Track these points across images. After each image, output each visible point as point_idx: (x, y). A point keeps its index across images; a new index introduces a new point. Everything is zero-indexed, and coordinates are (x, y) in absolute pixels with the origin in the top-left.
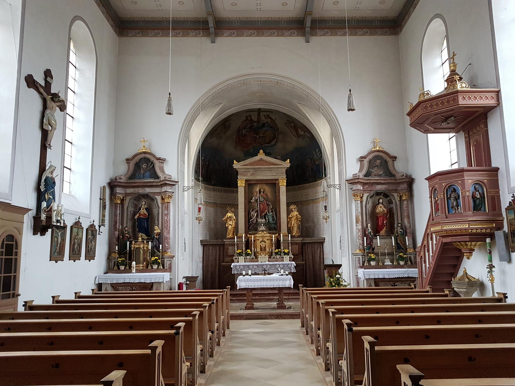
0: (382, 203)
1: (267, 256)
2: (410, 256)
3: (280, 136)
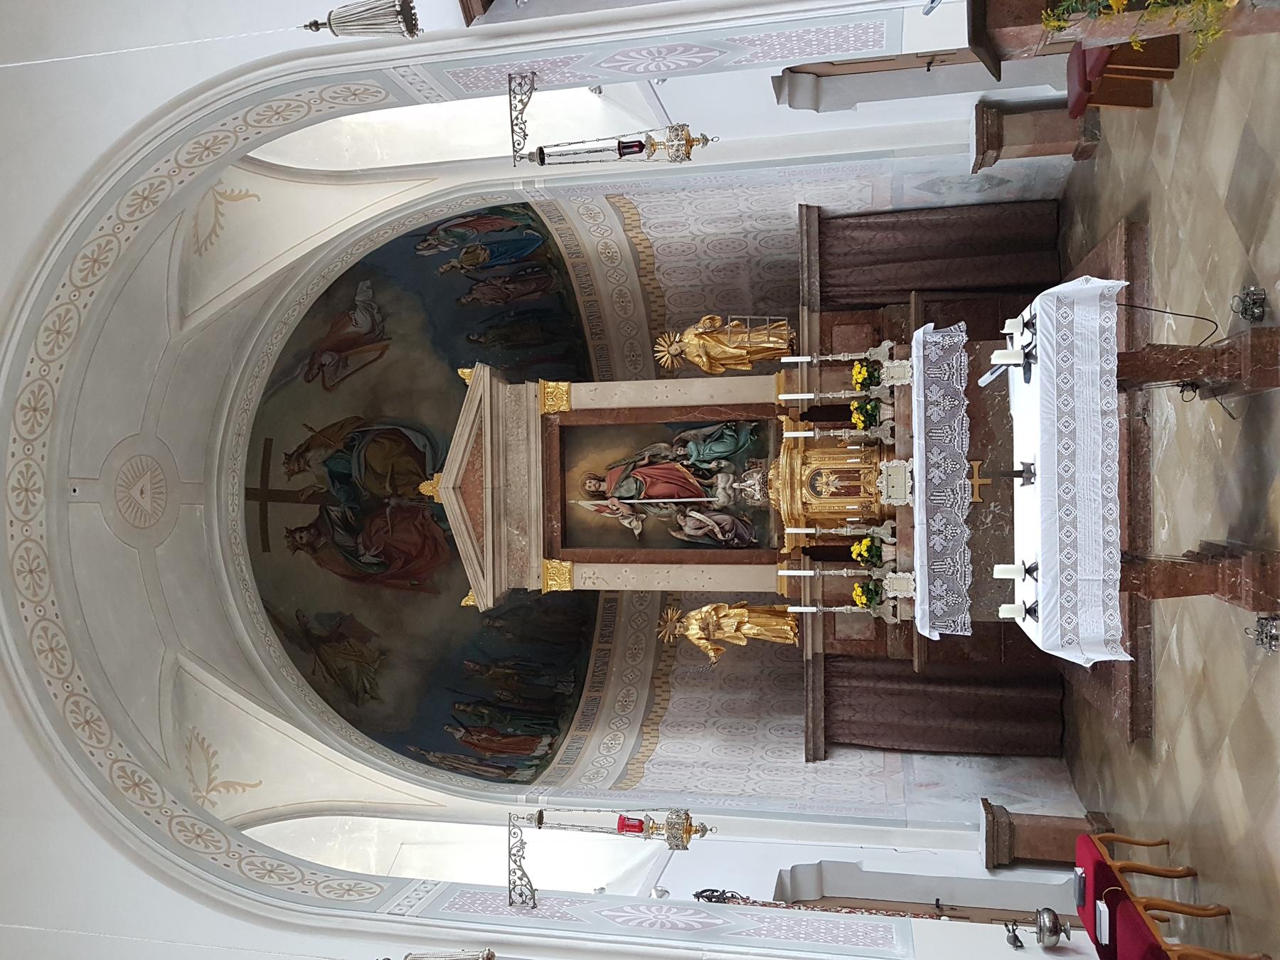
1: (883, 465)
3: (390, 411)
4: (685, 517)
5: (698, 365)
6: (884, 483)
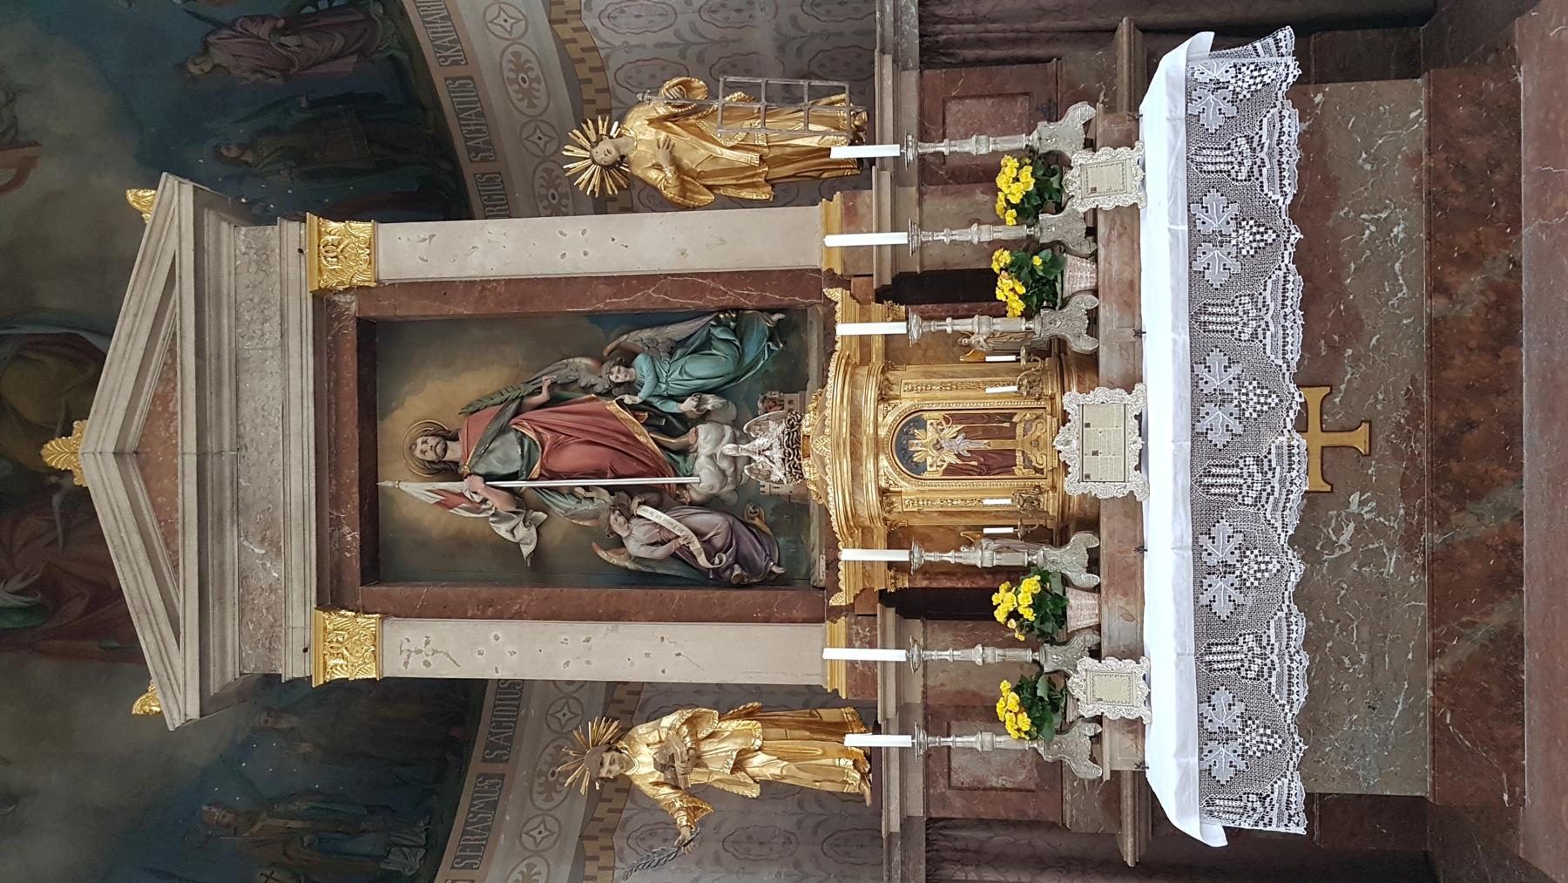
1: (1071, 400)
4: (628, 520)
5: (655, 188)
6: (1075, 443)
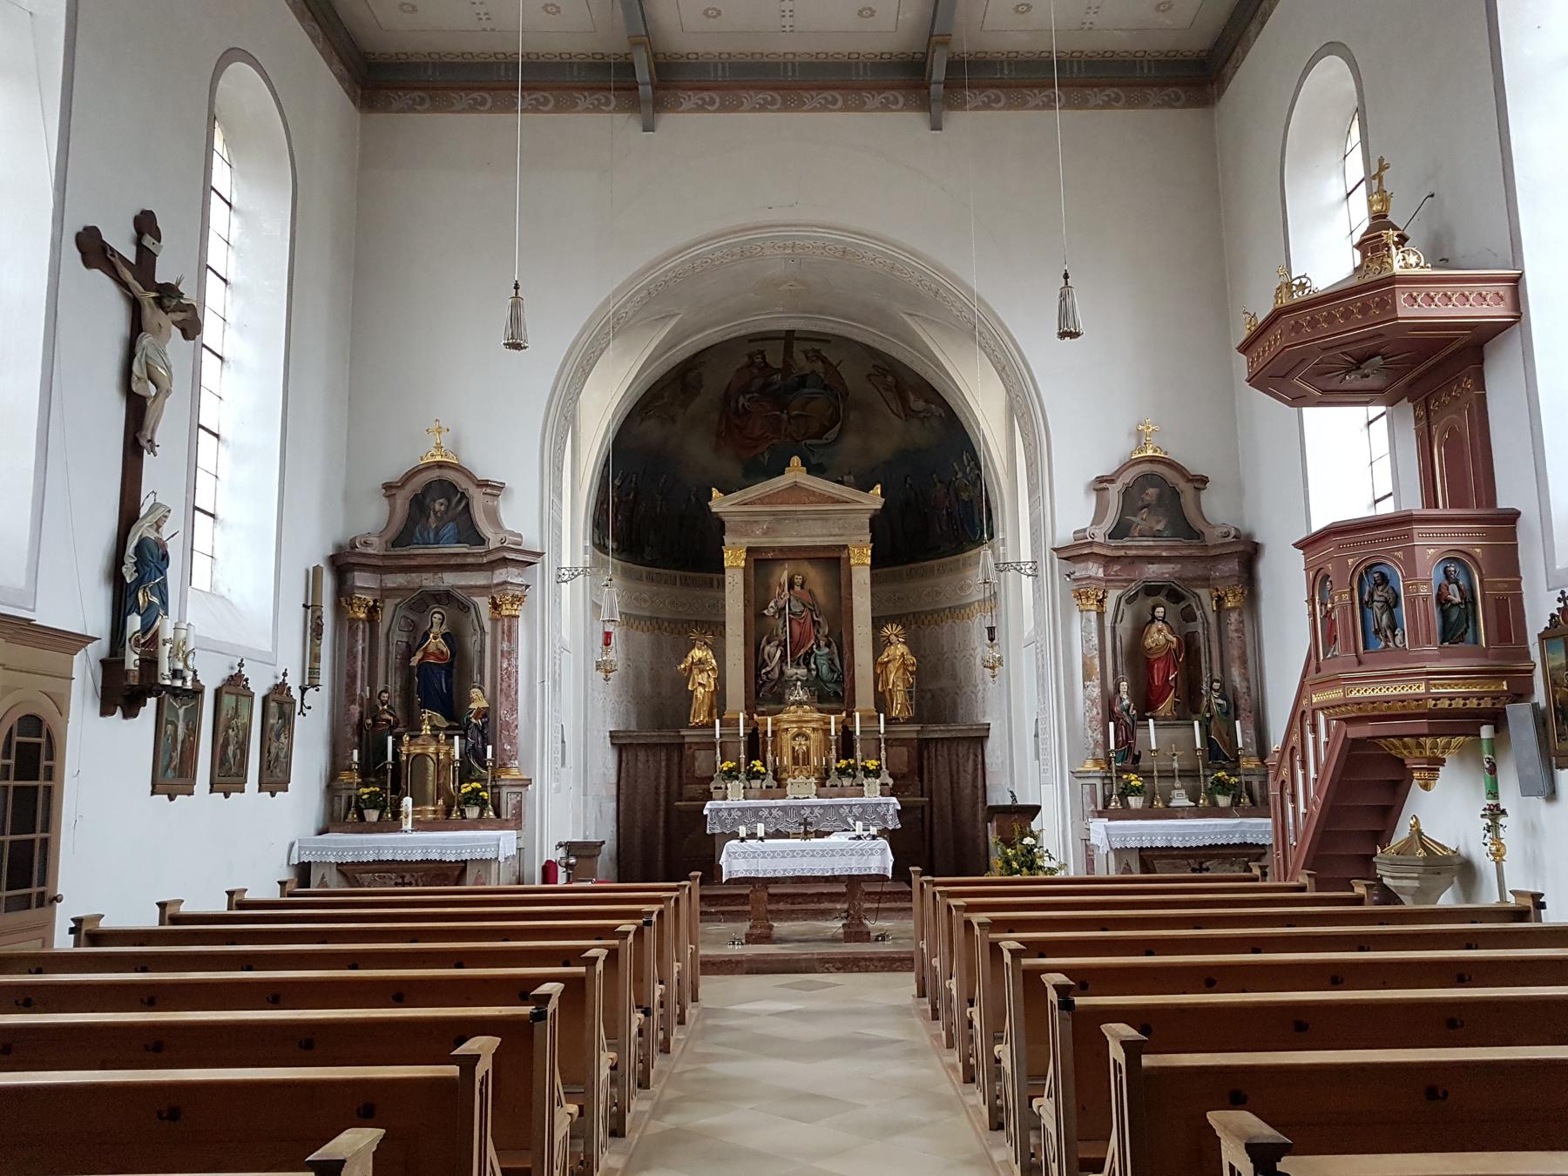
0: (1164, 617)
1: (813, 780)
2: (1249, 779)
3: (853, 415)
